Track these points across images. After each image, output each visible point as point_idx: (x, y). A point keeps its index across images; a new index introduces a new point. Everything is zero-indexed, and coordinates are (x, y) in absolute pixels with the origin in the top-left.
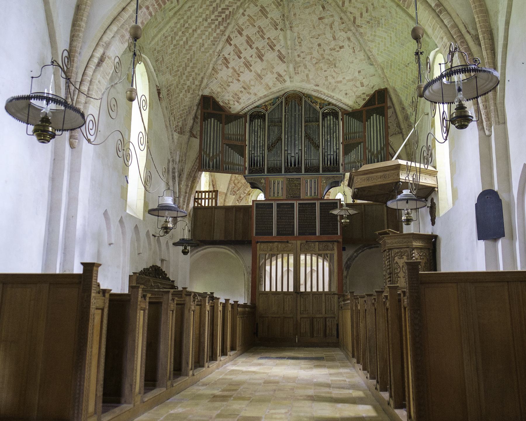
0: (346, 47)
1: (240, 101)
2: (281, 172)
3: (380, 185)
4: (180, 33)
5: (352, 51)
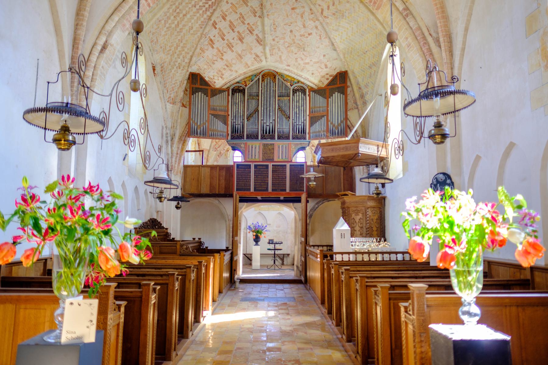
0: (314, 34)
1: (223, 77)
2: (258, 138)
3: (342, 155)
4: (172, 17)
5: (318, 37)
